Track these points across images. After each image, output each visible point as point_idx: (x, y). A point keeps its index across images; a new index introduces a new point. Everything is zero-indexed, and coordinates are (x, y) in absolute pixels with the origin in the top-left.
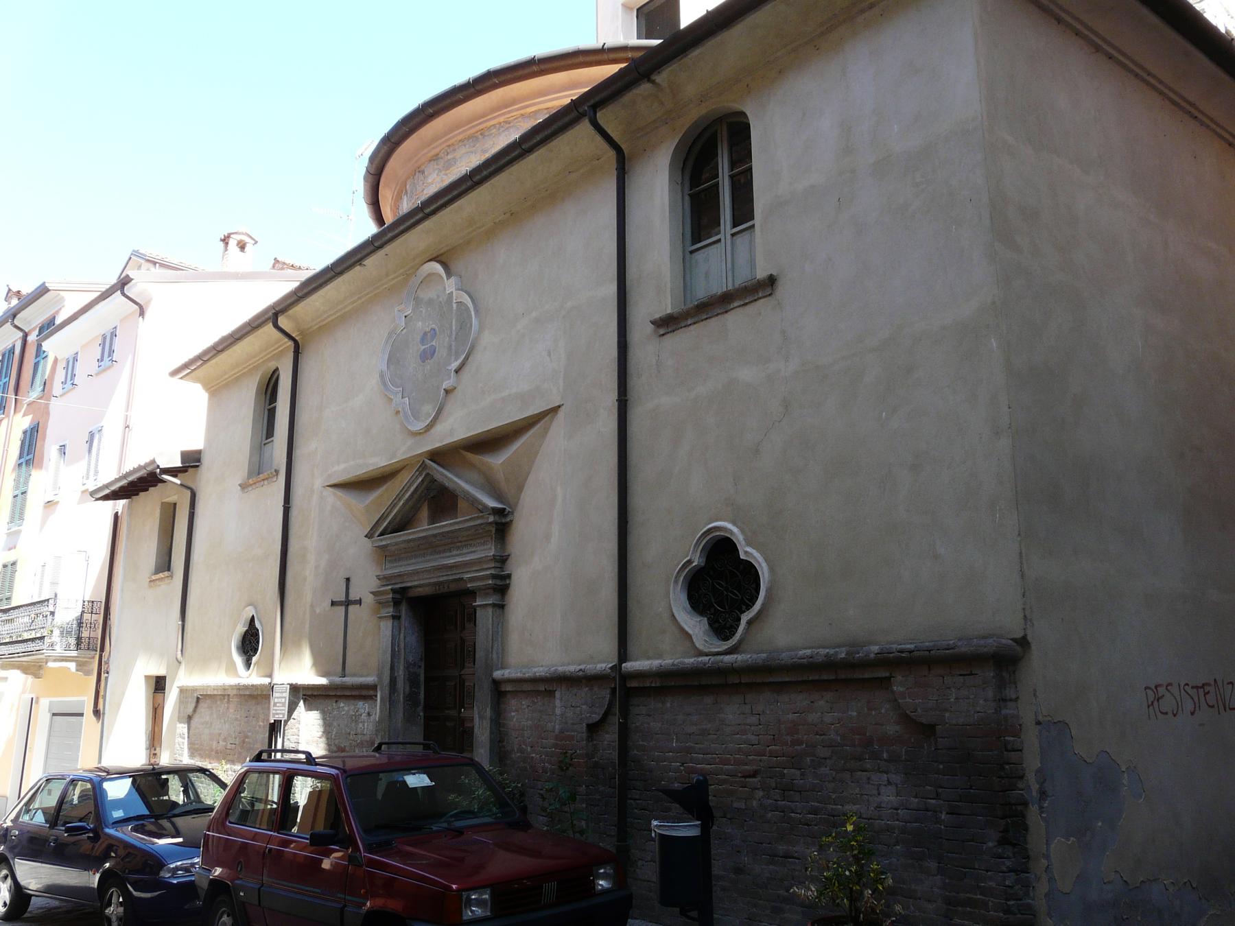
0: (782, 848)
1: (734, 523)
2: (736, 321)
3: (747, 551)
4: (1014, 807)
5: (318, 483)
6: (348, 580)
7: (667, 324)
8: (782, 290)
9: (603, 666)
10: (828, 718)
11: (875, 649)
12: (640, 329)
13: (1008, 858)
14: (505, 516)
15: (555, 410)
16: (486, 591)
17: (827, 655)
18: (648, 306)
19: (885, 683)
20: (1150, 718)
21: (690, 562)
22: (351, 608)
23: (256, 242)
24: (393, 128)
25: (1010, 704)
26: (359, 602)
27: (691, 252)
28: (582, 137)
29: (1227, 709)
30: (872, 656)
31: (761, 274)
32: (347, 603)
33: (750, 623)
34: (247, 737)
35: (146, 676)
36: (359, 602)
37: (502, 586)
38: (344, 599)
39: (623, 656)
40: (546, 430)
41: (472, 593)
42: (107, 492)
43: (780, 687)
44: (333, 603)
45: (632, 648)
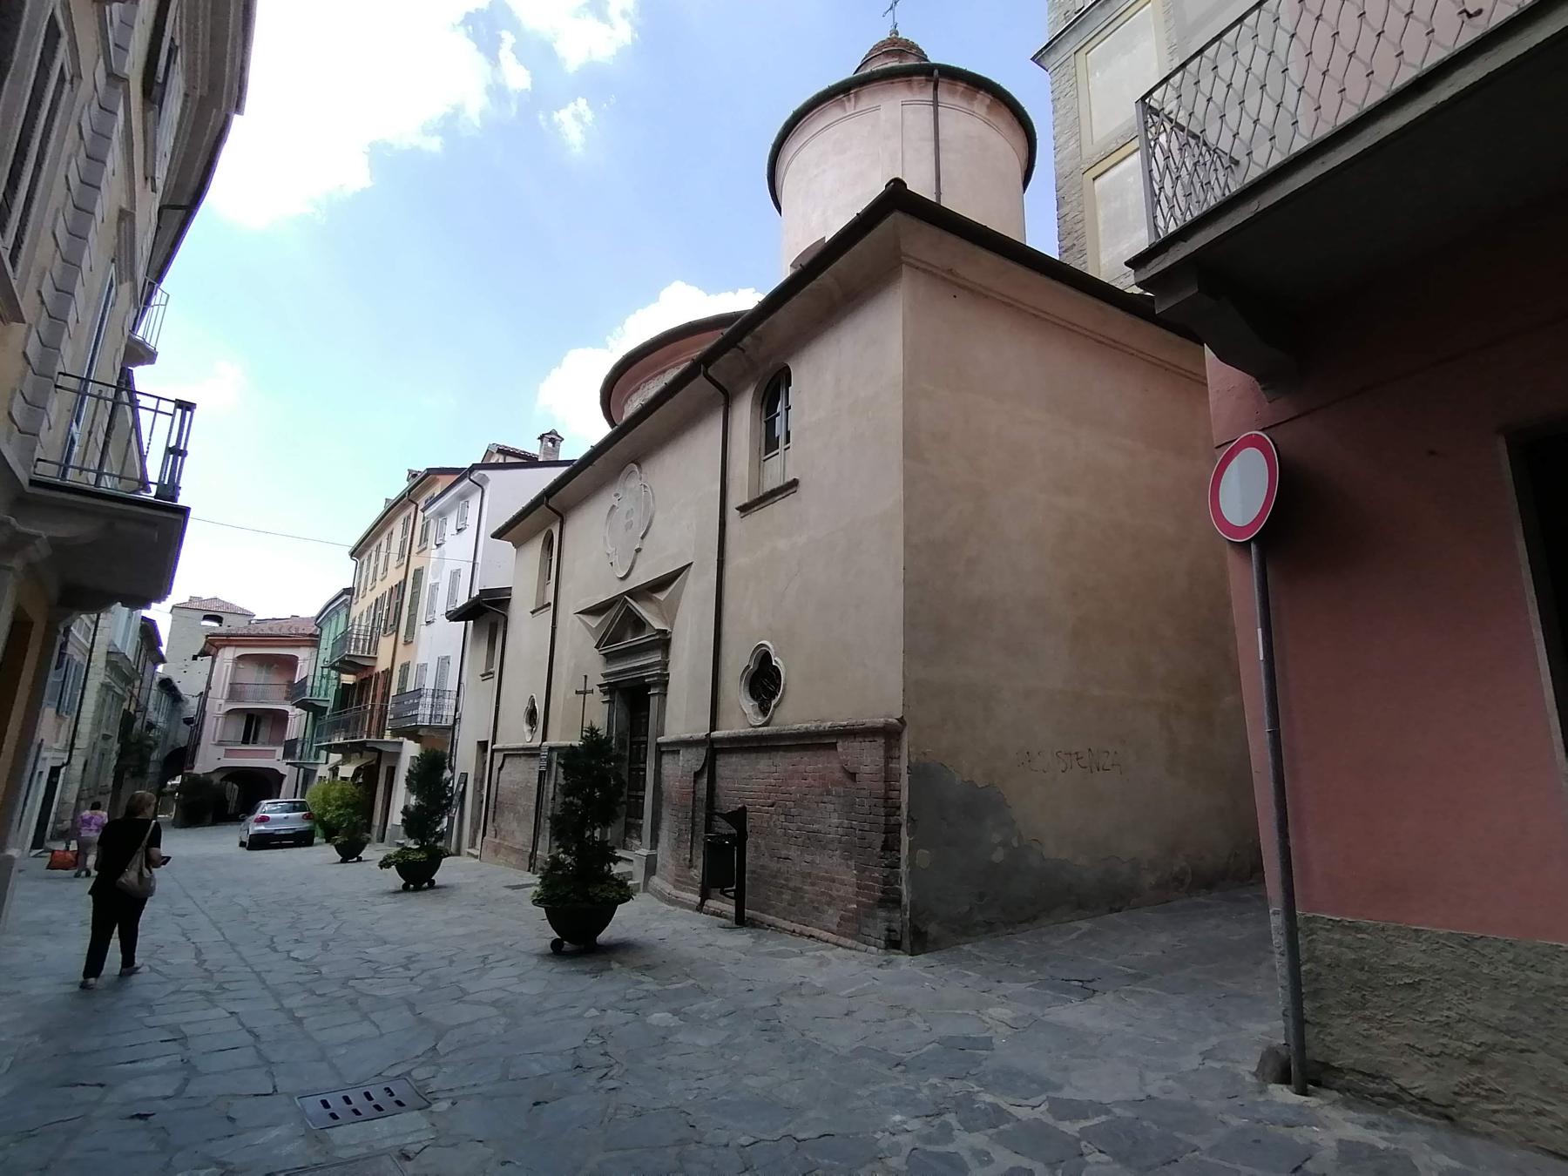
0: (784, 853)
1: (771, 642)
2: (779, 508)
3: (777, 661)
4: (427, 788)
5: (571, 612)
6: (586, 677)
7: (744, 509)
8: (801, 488)
9: (702, 734)
10: (809, 768)
11: (829, 724)
12: (732, 513)
13: (887, 859)
14: (667, 635)
15: (690, 565)
16: (654, 685)
17: (807, 728)
18: (738, 497)
19: (833, 746)
20: (1092, 772)
21: (748, 666)
22: (587, 695)
23: (563, 439)
24: (176, 563)
25: (894, 760)
26: (592, 692)
27: (764, 461)
28: (699, 384)
29: (1101, 769)
30: (827, 728)
31: (789, 479)
32: (585, 693)
33: (775, 707)
34: (528, 782)
35: (479, 742)
36: (592, 692)
37: (663, 682)
38: (583, 689)
39: (713, 728)
40: (686, 579)
41: (649, 686)
42: (455, 616)
43: (788, 749)
44: (577, 692)
45: (721, 721)
